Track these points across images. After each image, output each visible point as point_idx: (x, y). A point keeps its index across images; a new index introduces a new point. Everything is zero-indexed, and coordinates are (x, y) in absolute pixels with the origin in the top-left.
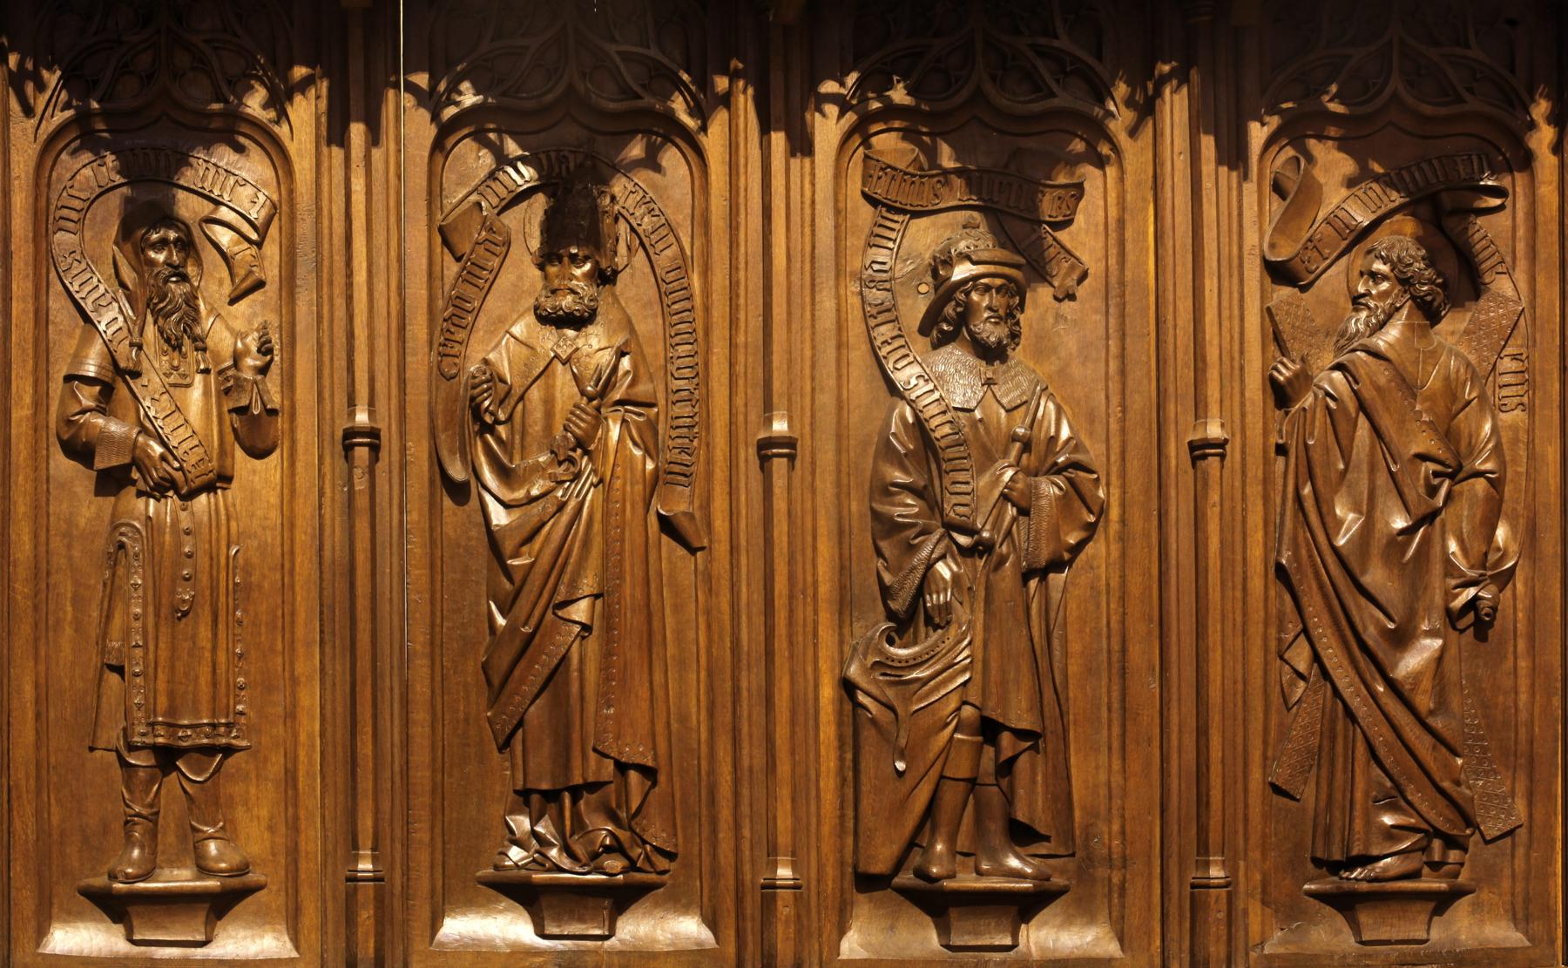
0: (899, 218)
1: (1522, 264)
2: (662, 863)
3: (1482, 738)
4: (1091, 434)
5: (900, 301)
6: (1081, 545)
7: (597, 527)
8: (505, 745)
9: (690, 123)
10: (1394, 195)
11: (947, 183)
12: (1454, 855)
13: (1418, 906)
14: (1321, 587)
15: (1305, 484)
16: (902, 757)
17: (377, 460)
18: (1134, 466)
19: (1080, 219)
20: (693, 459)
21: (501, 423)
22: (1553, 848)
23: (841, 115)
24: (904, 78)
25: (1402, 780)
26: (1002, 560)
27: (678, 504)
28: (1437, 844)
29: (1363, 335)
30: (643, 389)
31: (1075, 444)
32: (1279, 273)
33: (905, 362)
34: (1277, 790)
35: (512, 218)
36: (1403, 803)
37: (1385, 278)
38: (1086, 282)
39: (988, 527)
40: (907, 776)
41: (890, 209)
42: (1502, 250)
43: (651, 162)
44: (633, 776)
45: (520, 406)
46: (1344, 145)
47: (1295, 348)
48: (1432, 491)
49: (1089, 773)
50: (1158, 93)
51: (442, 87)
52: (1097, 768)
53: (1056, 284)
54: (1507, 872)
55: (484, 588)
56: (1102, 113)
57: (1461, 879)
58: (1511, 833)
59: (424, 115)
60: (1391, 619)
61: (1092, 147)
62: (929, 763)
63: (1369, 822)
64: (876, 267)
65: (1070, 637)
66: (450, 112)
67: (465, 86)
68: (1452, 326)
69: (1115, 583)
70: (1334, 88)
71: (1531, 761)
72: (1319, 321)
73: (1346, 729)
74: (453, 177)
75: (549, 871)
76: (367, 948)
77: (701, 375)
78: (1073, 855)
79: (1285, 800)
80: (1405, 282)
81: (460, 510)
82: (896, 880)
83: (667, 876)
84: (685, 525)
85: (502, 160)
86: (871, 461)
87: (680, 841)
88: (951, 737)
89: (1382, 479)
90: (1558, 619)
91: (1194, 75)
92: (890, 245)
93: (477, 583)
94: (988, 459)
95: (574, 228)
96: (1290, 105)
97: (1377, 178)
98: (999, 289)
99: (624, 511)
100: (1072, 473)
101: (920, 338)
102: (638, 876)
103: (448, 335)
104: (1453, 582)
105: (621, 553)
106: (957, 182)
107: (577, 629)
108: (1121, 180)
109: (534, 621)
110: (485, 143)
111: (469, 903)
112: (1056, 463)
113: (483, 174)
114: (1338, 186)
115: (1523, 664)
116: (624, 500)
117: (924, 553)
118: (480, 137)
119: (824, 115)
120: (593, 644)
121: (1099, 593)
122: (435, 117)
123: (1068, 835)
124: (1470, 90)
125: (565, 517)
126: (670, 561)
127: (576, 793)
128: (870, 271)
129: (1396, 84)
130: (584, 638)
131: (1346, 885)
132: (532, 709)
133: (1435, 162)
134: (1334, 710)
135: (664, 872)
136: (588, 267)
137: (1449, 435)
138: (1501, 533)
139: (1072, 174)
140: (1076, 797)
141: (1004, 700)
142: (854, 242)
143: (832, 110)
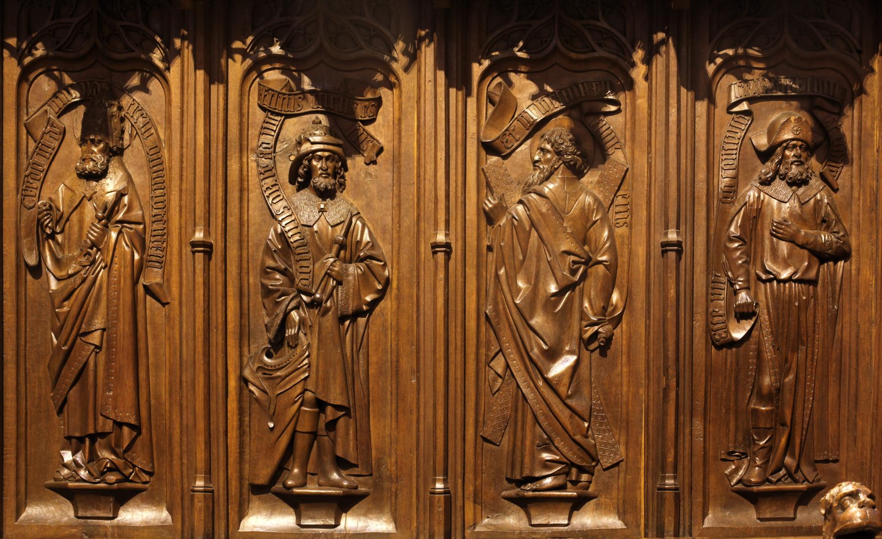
0: (278, 118)
1: (628, 144)
2: (146, 478)
3: (603, 411)
4: (384, 240)
5: (278, 165)
6: (374, 304)
7: (104, 291)
8: (60, 412)
9: (161, 65)
10: (557, 104)
11: (305, 98)
12: (584, 477)
13: (563, 505)
14: (510, 326)
15: (501, 268)
16: (272, 420)
17: (210, 258)
18: (404, 257)
19: (380, 118)
20: (164, 253)
21: (58, 233)
22: (639, 473)
23: (244, 60)
24: (280, 39)
25: (553, 435)
26: (327, 310)
27: (153, 277)
28: (574, 471)
29: (536, 184)
30: (137, 213)
31: (373, 245)
32: (490, 148)
33: (278, 199)
34: (485, 439)
35: (66, 120)
36: (553, 448)
37: (548, 151)
38: (382, 154)
39: (319, 292)
40: (275, 430)
41: (273, 113)
42: (619, 136)
43: (143, 87)
44: (126, 430)
45: (68, 224)
46: (530, 76)
47: (498, 191)
48: (573, 272)
49: (380, 429)
50: (419, 48)
51: (24, 46)
52: (385, 426)
53: (366, 155)
54: (615, 486)
55: (49, 325)
56: (388, 58)
57: (590, 490)
58: (617, 464)
59: (14, 62)
60: (546, 344)
61: (386, 78)
62: (286, 423)
63: (533, 458)
64: (264, 146)
65: (370, 354)
66: (28, 60)
67: (39, 45)
68: (590, 178)
69: (394, 324)
70: (521, 44)
71: (627, 423)
72: (514, 176)
73: (523, 406)
74: (804, 119)
75: (77, 481)
76: (200, 527)
77: (166, 208)
78: (371, 475)
79: (491, 445)
80: (559, 153)
81: (36, 282)
82: (274, 488)
83: (147, 485)
84: (157, 289)
85: (62, 87)
86: (261, 255)
87: (156, 465)
88: (299, 409)
89: (544, 265)
90: (643, 344)
91: (435, 37)
92: (273, 133)
93: (45, 322)
94: (320, 253)
95: (100, 127)
96: (497, 53)
97: (548, 95)
98: (327, 158)
99: (120, 282)
100: (368, 262)
101: (290, 186)
102: (128, 485)
103: (28, 185)
104: (584, 323)
105: (118, 305)
106: (311, 98)
107: (92, 347)
108: (400, 96)
109: (69, 343)
110: (53, 77)
111: (40, 499)
112: (359, 256)
113: (50, 94)
114: (527, 98)
115: (625, 369)
116: (120, 276)
117: (283, 306)
118: (49, 73)
119: (234, 60)
120: (102, 357)
121: (387, 329)
122: (20, 63)
123: (368, 464)
124: (600, 45)
125: (85, 286)
126: (151, 311)
127: (93, 438)
128: (261, 149)
129: (556, 41)
130: (97, 353)
131: (521, 493)
132: (71, 391)
133: (580, 86)
134: (517, 395)
135: (146, 483)
136: (102, 145)
137: (585, 241)
138: (615, 297)
139: (375, 93)
140: (373, 442)
141: (326, 389)
142: (253, 132)
143: (238, 57)
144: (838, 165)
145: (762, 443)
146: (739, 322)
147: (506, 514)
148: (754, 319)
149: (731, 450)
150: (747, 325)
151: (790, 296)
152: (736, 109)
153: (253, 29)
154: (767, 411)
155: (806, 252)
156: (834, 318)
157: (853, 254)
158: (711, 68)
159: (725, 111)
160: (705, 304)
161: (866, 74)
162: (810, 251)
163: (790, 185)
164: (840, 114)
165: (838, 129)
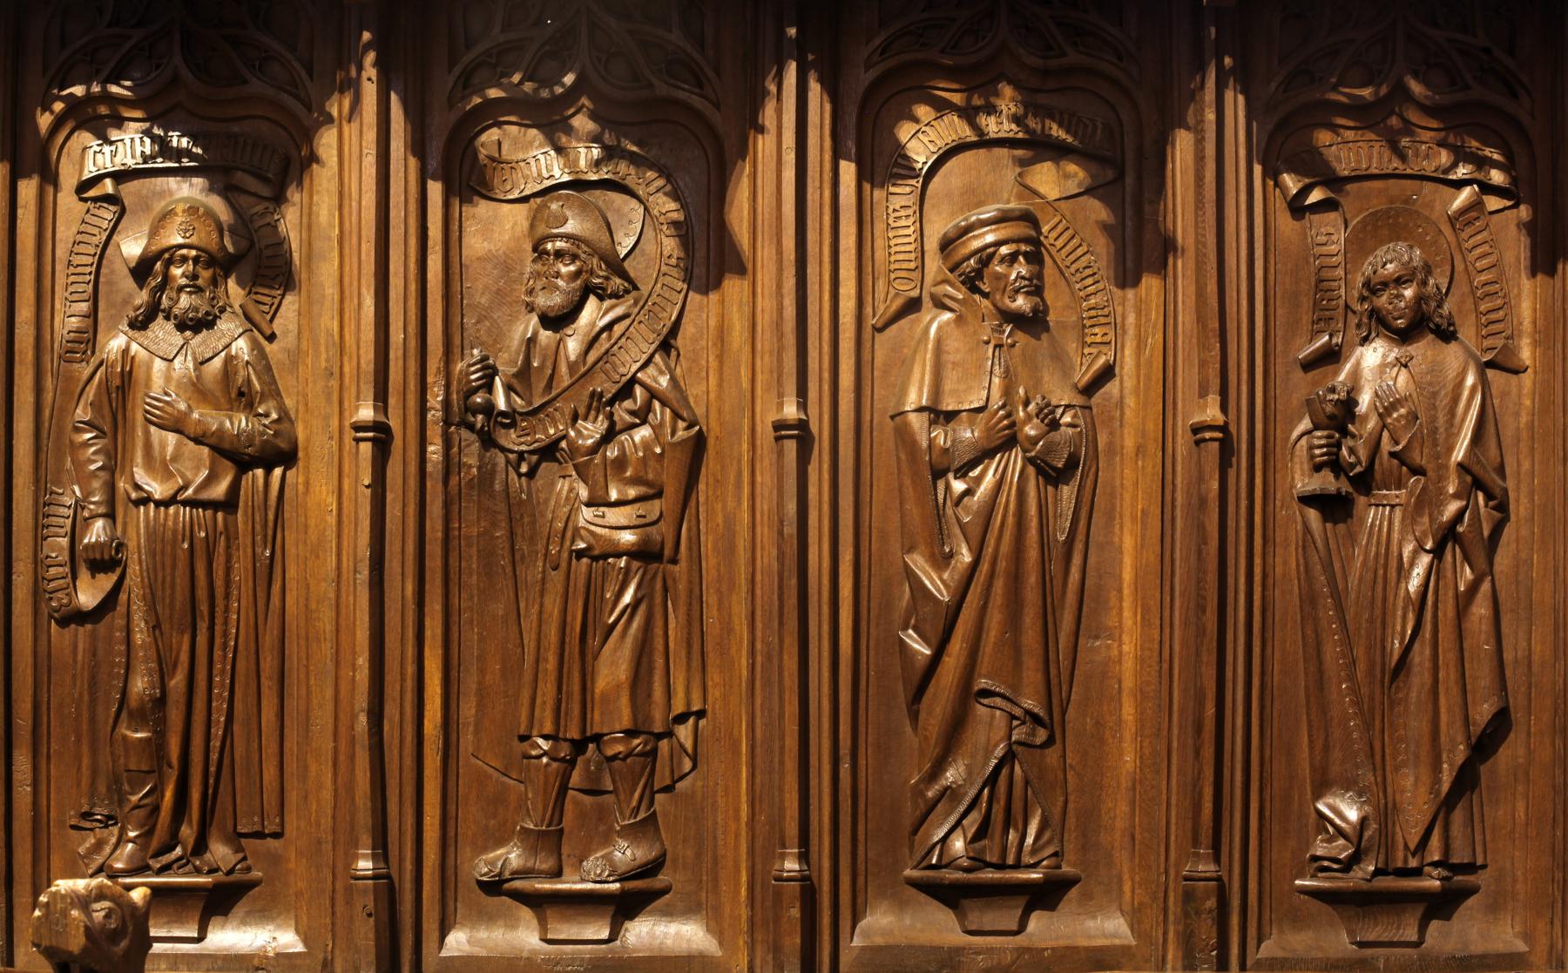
144: (274, 293)
145: (134, 798)
146: (93, 577)
147: (513, 925)
148: (119, 571)
149: (85, 808)
150: (107, 581)
151: (175, 531)
152: (92, 193)
153: (98, 72)
154: (140, 739)
155: (206, 450)
156: (268, 572)
157: (300, 454)
158: (45, 121)
159: (75, 197)
160: (31, 544)
161: (318, 125)
162: (213, 448)
163: (181, 327)
164: (279, 199)
165: (274, 227)
